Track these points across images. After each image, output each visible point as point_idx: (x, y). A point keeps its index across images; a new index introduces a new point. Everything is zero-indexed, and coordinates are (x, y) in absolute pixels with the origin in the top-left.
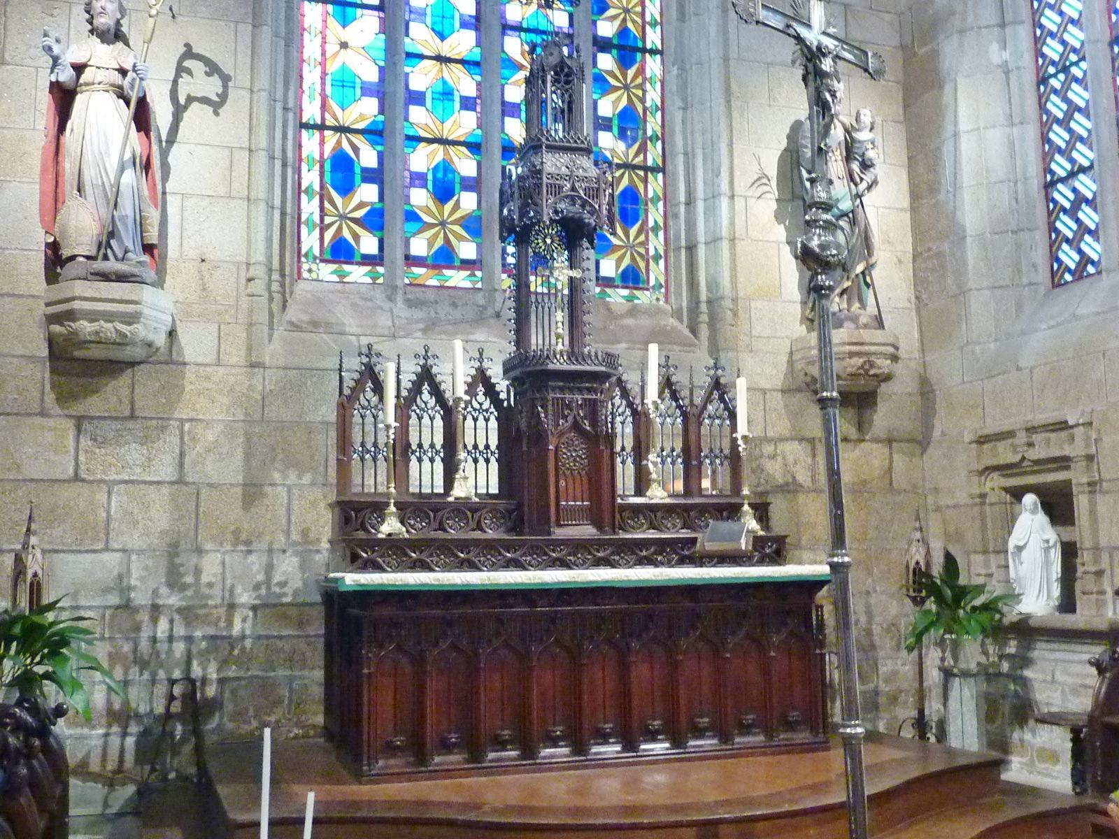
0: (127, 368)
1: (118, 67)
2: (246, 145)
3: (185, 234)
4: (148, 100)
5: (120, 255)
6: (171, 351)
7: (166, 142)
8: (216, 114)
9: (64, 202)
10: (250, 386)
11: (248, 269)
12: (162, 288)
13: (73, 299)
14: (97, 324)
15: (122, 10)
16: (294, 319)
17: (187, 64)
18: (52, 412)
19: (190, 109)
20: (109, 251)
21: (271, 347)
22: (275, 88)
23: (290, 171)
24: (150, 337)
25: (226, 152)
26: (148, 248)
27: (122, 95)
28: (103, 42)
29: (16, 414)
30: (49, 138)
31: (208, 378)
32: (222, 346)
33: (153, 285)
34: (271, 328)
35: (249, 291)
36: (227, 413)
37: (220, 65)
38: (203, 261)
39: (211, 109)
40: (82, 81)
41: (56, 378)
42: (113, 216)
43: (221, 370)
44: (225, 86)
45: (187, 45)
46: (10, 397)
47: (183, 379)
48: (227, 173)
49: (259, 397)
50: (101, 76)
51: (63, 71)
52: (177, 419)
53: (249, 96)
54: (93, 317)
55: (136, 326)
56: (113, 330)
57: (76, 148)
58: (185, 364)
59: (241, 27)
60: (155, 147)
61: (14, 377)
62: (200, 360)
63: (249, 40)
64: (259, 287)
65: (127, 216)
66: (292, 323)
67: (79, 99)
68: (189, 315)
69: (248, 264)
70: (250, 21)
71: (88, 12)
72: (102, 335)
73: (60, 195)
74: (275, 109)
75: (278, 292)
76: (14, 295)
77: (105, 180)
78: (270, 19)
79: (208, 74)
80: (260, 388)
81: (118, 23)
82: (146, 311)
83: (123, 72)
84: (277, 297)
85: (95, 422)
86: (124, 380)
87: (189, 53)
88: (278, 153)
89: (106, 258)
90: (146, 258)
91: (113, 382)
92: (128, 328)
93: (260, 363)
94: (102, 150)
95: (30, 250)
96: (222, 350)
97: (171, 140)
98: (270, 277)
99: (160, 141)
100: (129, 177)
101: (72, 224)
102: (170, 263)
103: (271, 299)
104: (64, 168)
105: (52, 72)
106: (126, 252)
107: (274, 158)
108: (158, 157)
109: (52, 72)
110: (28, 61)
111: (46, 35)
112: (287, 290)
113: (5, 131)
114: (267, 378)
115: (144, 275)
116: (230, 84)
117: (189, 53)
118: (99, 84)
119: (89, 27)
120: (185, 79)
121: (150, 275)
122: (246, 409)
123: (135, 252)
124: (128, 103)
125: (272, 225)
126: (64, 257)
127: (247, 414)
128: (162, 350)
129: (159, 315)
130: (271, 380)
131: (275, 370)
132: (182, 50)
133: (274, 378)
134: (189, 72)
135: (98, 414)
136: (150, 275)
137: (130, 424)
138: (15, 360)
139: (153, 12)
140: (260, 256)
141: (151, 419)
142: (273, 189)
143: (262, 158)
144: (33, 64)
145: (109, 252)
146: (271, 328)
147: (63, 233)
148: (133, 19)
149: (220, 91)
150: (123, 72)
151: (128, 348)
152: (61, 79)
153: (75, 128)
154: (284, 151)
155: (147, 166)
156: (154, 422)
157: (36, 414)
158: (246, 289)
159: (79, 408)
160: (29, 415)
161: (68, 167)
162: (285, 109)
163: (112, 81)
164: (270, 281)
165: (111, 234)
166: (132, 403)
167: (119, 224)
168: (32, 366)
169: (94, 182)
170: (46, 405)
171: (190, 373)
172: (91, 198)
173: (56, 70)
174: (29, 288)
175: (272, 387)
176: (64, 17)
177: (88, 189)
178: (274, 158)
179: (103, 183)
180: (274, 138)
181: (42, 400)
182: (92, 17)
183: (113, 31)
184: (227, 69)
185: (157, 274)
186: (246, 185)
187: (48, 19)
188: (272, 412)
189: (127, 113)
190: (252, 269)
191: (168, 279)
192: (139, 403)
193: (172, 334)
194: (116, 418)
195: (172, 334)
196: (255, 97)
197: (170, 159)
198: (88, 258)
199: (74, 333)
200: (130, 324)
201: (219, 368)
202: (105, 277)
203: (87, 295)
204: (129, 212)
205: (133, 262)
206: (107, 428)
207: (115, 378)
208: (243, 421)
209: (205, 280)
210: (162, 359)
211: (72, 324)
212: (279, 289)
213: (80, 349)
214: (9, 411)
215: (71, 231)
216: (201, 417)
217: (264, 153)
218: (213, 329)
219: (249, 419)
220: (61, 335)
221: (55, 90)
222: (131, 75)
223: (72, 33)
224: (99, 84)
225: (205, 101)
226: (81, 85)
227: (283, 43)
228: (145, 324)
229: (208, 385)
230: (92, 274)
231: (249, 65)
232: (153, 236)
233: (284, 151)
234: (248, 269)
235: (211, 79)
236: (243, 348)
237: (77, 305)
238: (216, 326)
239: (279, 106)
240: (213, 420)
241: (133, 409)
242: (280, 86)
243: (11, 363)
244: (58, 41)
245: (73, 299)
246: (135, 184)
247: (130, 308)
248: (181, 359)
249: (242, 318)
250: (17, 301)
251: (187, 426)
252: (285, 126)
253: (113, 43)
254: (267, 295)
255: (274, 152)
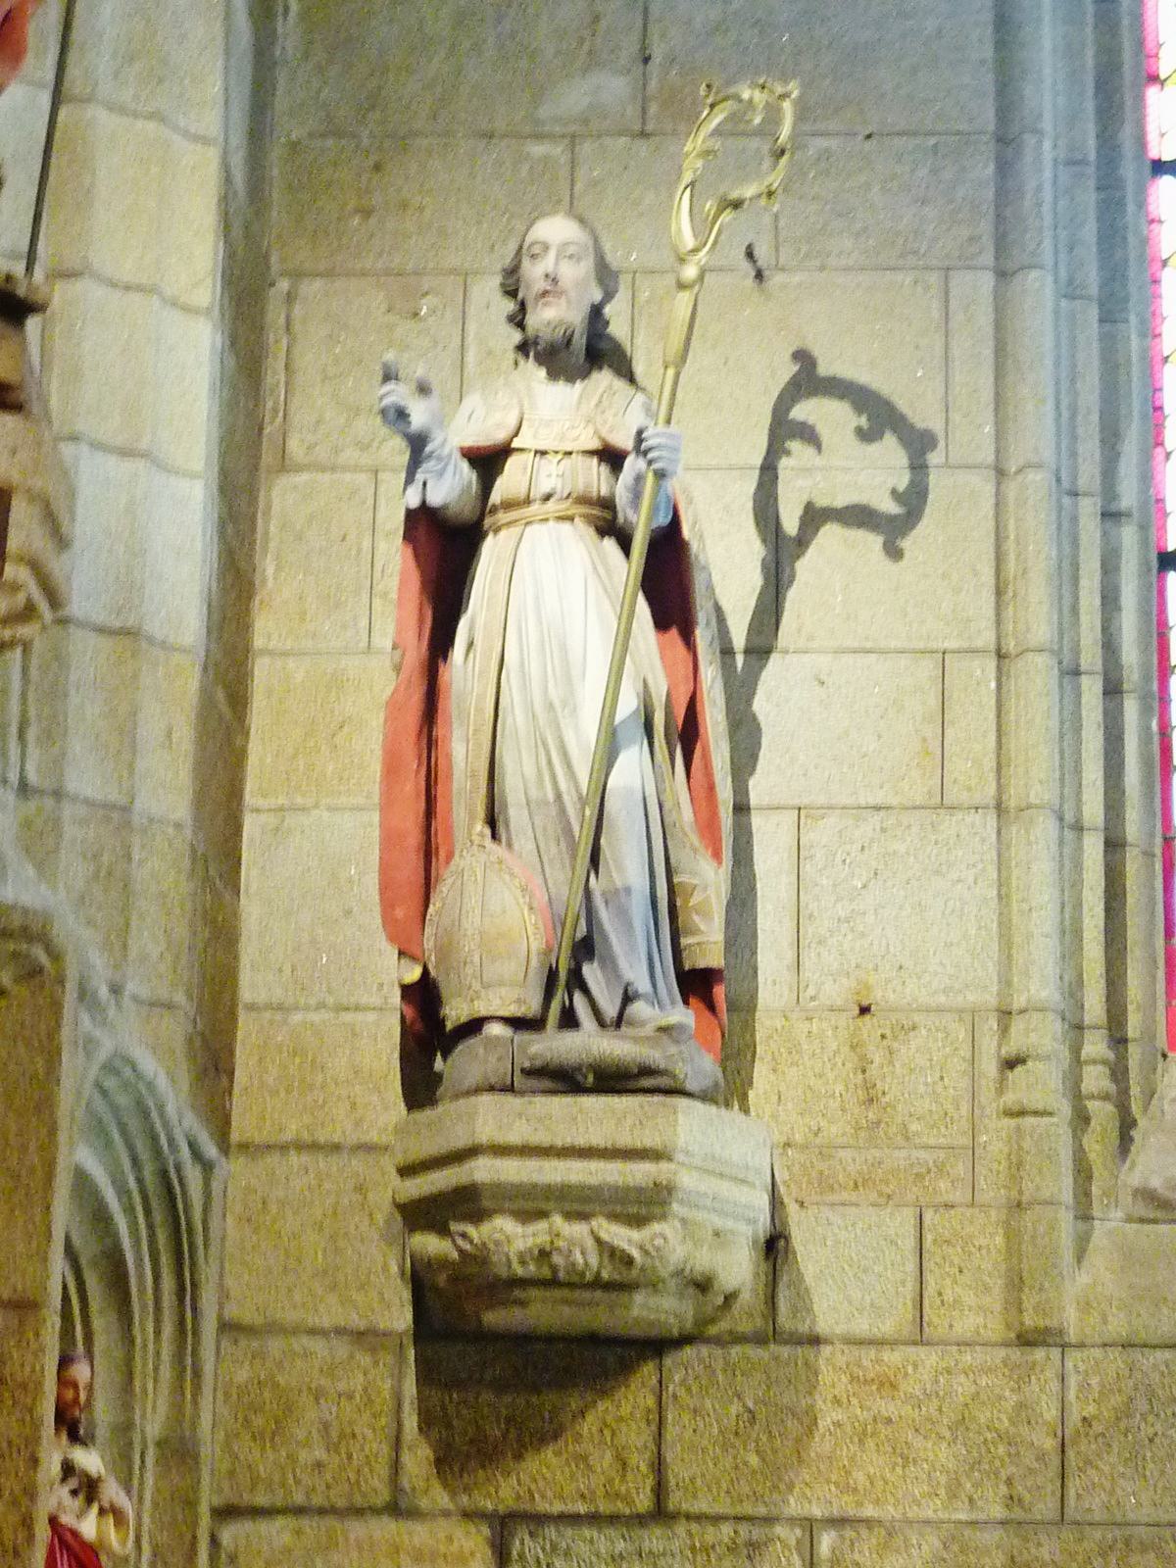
0: (643, 1358)
1: (595, 444)
2: (987, 638)
3: (809, 931)
4: (686, 532)
5: (610, 1010)
6: (771, 1300)
7: (747, 652)
8: (894, 552)
9: (450, 856)
10: (1021, 1406)
11: (1004, 1030)
12: (745, 1110)
13: (472, 1152)
14: (542, 1225)
15: (606, 276)
16: (1156, 1183)
17: (801, 412)
18: (424, 1503)
19: (812, 551)
20: (578, 997)
21: (1083, 1279)
22: (1074, 455)
23: (1131, 708)
24: (703, 1260)
25: (928, 668)
26: (696, 984)
27: (610, 526)
28: (553, 375)
29: (322, 1511)
30: (404, 674)
31: (887, 1384)
32: (929, 1278)
33: (706, 1097)
34: (1084, 1216)
35: (1010, 1098)
36: (953, 1496)
37: (902, 405)
38: (864, 1010)
39: (874, 541)
40: (495, 497)
41: (435, 1396)
42: (588, 894)
43: (930, 1358)
44: (919, 467)
45: (804, 358)
46: (304, 1456)
47: (812, 1388)
48: (932, 731)
49: (1050, 1444)
50: (550, 476)
51: (441, 474)
52: (792, 1521)
53: (990, 489)
54: (531, 1204)
55: (656, 1227)
56: (590, 1243)
57: (481, 697)
58: (815, 1341)
59: (961, 281)
60: (710, 675)
61: (318, 1395)
62: (862, 1326)
63: (985, 318)
64: (1041, 1084)
65: (628, 890)
66: (1147, 1195)
67: (491, 551)
68: (826, 1184)
69: (1005, 1014)
70: (988, 258)
71: (511, 293)
72: (557, 1259)
73: (440, 839)
74: (1074, 519)
75: (1106, 1097)
76: (314, 1147)
77: (563, 785)
78: (1047, 244)
79: (866, 436)
80: (1051, 1413)
81: (596, 313)
82: (687, 1180)
83: (611, 457)
84: (1102, 1112)
85: (551, 1532)
86: (635, 1396)
87: (807, 379)
88: (1091, 656)
89: (569, 1020)
90: (682, 1015)
91: (602, 1406)
92: (636, 1235)
93: (1047, 1330)
94: (554, 694)
95: (357, 1008)
96: (930, 1290)
97: (760, 650)
98: (1076, 1050)
99: (727, 652)
100: (632, 769)
101: (472, 923)
102: (765, 1023)
103: (1082, 1119)
104: (449, 756)
105: (410, 479)
106: (628, 998)
107: (1076, 673)
108: (721, 702)
109: (410, 479)
110: (350, 455)
111: (388, 376)
112: (1135, 1090)
113: (291, 664)
114: (1073, 1381)
115: (681, 1070)
116: (934, 458)
117: (807, 379)
118: (547, 498)
119: (517, 337)
120: (797, 456)
121: (699, 1065)
122: (1009, 1482)
123: (655, 999)
124: (625, 545)
125: (1077, 884)
126: (449, 1026)
127: (1011, 1500)
128: (746, 1296)
129: (726, 1189)
130: (1084, 1386)
131: (1097, 1353)
132: (788, 370)
133: (1094, 1381)
134: (809, 435)
135: (557, 1508)
136: (699, 1065)
137: (654, 1539)
138: (318, 1346)
139: (690, 272)
140: (1040, 984)
141: (717, 1519)
142: (1078, 771)
143: (1037, 677)
144: (366, 460)
145: (579, 1002)
146: (1084, 1216)
147: (444, 952)
148: (644, 295)
149: (903, 481)
150: (611, 457)
151: (639, 1298)
152: (435, 499)
153: (478, 643)
154: (1110, 646)
155: (688, 734)
156: (726, 1530)
157: (376, 1511)
158: (1001, 1090)
159: (504, 1491)
160: (358, 1512)
161: (462, 752)
162: (1111, 516)
163: (580, 488)
164: (1077, 1062)
165: (586, 948)
166: (659, 1466)
167: (604, 914)
168: (365, 1360)
169: (534, 793)
170: (405, 1483)
171: (831, 1368)
172: (524, 843)
173: (420, 477)
174: (358, 1124)
175: (1091, 1410)
176: (448, 315)
177: (516, 814)
178: (1076, 673)
179: (559, 796)
180: (1075, 610)
181: (396, 1466)
182: (523, 307)
183: (580, 342)
184: (924, 415)
185: (724, 1062)
186: (989, 763)
187: (405, 328)
188: (1089, 1498)
189: (623, 570)
190: (1017, 1026)
191: (761, 1073)
192: (679, 1471)
193: (774, 1247)
194: (613, 1519)
195: (774, 1247)
196: (1011, 489)
197: (760, 705)
198: (517, 1023)
199: (477, 1259)
200: (638, 1221)
201: (922, 1351)
202: (564, 1079)
203: (514, 1138)
204: (637, 878)
205: (649, 1030)
206: (583, 1549)
207: (604, 1393)
208: (1003, 1523)
209: (873, 1071)
210: (745, 1327)
211: (471, 1230)
212: (1108, 1085)
213: (504, 1304)
214: (299, 1498)
215: (469, 947)
216: (869, 1511)
217: (1041, 661)
218: (901, 1224)
219: (1018, 1513)
220: (444, 1263)
221: (421, 532)
222: (632, 465)
223: (471, 357)
224: (547, 498)
225: (859, 516)
226: (494, 510)
227: (1094, 313)
228: (684, 1221)
229: (887, 1407)
230: (528, 1073)
231: (987, 394)
232: (708, 946)
233: (1110, 646)
234: (1004, 1030)
235: (874, 448)
236: (998, 1284)
237: (483, 1170)
238: (909, 1215)
239: (1089, 509)
240: (909, 1522)
241: (660, 1490)
242: (1090, 449)
243: (307, 1355)
244: (423, 389)
245: (472, 1152)
246: (651, 791)
247: (639, 1173)
248: (803, 1328)
249: (991, 1191)
250: (322, 1162)
251: (826, 1542)
252: (1110, 566)
253: (584, 375)
254: (1065, 1109)
255: (1076, 651)
